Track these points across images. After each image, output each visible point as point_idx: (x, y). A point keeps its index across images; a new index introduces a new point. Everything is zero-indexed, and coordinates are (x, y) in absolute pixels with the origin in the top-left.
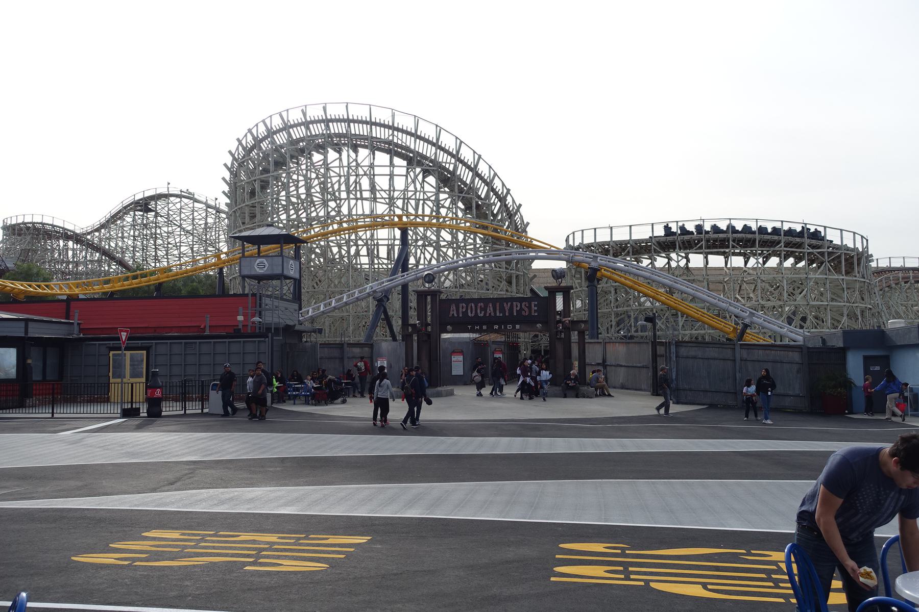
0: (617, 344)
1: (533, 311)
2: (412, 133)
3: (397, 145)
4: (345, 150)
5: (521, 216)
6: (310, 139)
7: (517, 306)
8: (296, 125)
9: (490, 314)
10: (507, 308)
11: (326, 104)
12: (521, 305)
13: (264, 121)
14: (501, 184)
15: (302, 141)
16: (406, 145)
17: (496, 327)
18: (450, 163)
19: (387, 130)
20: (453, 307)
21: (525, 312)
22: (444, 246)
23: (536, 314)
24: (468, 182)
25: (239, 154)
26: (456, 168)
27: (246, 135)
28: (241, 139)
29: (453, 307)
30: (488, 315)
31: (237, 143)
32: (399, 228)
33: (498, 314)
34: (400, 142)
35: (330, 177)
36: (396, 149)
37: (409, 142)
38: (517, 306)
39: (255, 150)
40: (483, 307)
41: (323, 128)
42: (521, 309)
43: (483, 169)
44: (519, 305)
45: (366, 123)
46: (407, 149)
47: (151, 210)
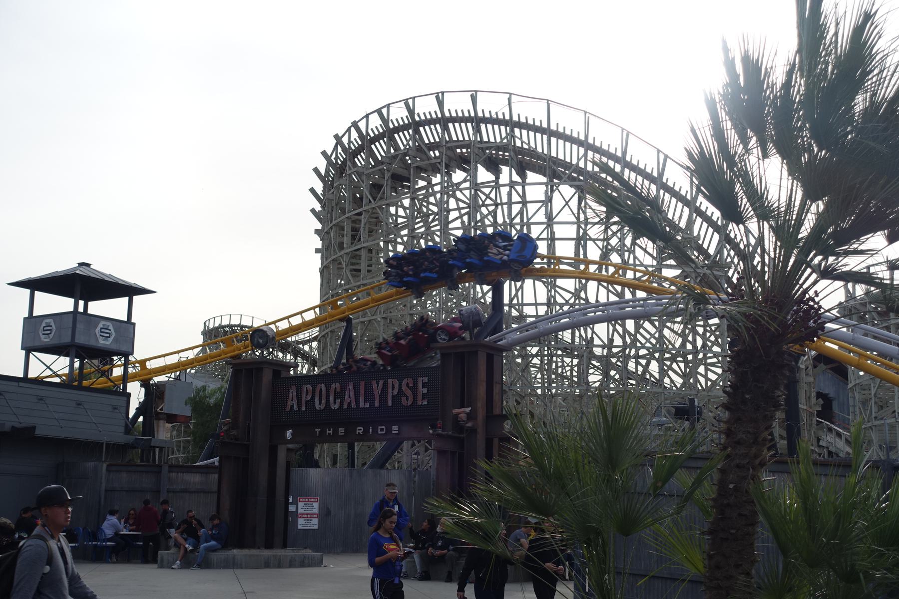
1: (420, 397)
2: (617, 157)
4: (505, 170)
6: (447, 146)
7: (393, 388)
8: (377, 138)
9: (349, 404)
10: (377, 391)
11: (476, 92)
13: (406, 102)
16: (530, 147)
17: (360, 430)
19: (575, 147)
20: (293, 393)
21: (407, 399)
22: (667, 359)
23: (425, 403)
24: (712, 251)
26: (690, 223)
27: (349, 130)
28: (340, 135)
29: (293, 393)
30: (345, 406)
33: (362, 405)
38: (393, 388)
39: (362, 154)
40: (338, 390)
41: (504, 135)
44: (397, 386)
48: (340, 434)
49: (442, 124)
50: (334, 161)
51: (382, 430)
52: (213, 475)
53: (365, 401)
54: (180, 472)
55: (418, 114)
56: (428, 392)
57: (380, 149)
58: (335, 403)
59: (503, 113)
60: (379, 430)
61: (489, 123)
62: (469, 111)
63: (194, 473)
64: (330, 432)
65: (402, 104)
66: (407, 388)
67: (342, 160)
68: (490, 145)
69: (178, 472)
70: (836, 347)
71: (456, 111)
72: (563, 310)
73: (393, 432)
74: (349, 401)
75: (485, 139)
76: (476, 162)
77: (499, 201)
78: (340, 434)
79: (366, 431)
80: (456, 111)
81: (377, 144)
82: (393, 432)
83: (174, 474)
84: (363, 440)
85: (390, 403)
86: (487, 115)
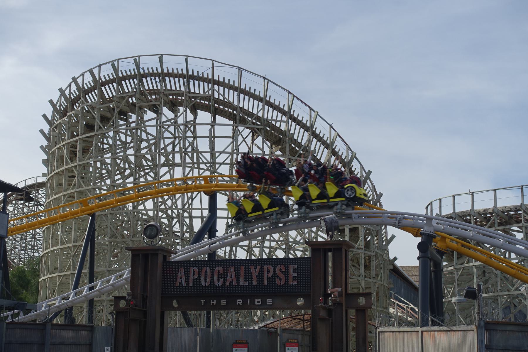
0: (436, 333)
1: (291, 279)
3: (217, 101)
5: (373, 186)
7: (268, 271)
9: (231, 282)
12: (274, 271)
13: (91, 71)
14: (345, 148)
15: (155, 94)
17: (239, 302)
18: (281, 121)
20: (181, 273)
21: (281, 280)
23: (296, 283)
25: (61, 105)
27: (70, 85)
29: (181, 273)
30: (228, 284)
31: (59, 93)
32: (206, 193)
33: (242, 283)
34: (221, 98)
35: (164, 138)
36: (217, 105)
37: (232, 96)
38: (268, 271)
40: (221, 272)
42: (275, 275)
43: (321, 128)
44: (272, 270)
45: (182, 76)
46: (230, 105)
47: (32, 199)
48: (222, 304)
49: (138, 79)
50: (58, 108)
51: (258, 302)
52: (82, 332)
53: (245, 281)
54: (59, 330)
55: (121, 71)
56: (297, 276)
57: (92, 98)
58: (218, 281)
59: (208, 74)
60: (256, 302)
61: (197, 80)
62: (182, 70)
63: (68, 330)
64: (213, 302)
65: (109, 66)
66: (280, 272)
67: (64, 107)
68: (196, 96)
69: (56, 330)
70: (523, 248)
71: (177, 69)
72: (205, 217)
73: (268, 304)
74: (231, 280)
75: (192, 90)
76: (187, 106)
77: (177, 135)
78: (222, 304)
79: (245, 302)
80: (173, 69)
81: (90, 94)
82: (268, 304)
83: (54, 331)
84: (242, 309)
85: (266, 283)
86: (195, 74)
